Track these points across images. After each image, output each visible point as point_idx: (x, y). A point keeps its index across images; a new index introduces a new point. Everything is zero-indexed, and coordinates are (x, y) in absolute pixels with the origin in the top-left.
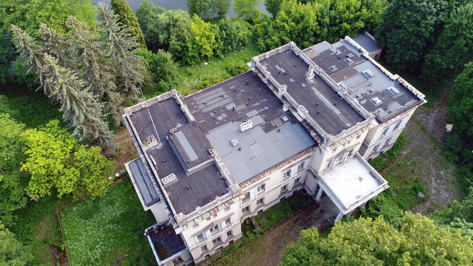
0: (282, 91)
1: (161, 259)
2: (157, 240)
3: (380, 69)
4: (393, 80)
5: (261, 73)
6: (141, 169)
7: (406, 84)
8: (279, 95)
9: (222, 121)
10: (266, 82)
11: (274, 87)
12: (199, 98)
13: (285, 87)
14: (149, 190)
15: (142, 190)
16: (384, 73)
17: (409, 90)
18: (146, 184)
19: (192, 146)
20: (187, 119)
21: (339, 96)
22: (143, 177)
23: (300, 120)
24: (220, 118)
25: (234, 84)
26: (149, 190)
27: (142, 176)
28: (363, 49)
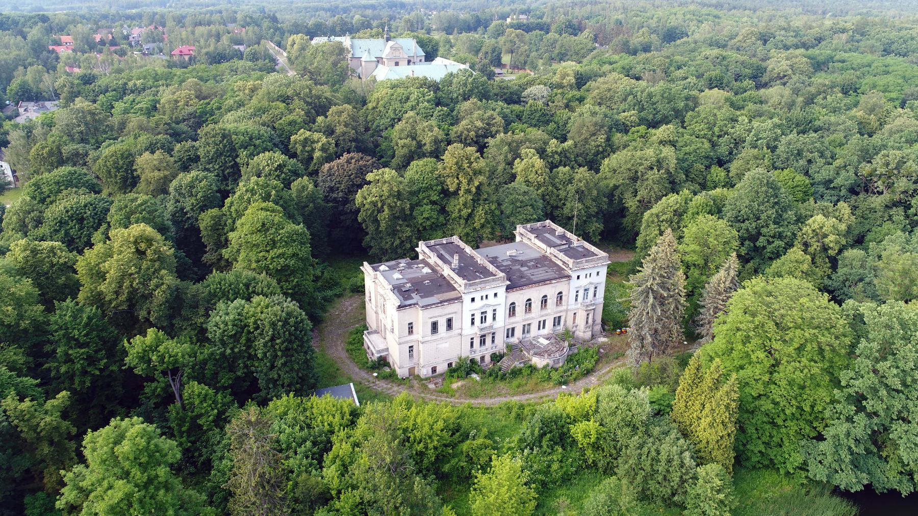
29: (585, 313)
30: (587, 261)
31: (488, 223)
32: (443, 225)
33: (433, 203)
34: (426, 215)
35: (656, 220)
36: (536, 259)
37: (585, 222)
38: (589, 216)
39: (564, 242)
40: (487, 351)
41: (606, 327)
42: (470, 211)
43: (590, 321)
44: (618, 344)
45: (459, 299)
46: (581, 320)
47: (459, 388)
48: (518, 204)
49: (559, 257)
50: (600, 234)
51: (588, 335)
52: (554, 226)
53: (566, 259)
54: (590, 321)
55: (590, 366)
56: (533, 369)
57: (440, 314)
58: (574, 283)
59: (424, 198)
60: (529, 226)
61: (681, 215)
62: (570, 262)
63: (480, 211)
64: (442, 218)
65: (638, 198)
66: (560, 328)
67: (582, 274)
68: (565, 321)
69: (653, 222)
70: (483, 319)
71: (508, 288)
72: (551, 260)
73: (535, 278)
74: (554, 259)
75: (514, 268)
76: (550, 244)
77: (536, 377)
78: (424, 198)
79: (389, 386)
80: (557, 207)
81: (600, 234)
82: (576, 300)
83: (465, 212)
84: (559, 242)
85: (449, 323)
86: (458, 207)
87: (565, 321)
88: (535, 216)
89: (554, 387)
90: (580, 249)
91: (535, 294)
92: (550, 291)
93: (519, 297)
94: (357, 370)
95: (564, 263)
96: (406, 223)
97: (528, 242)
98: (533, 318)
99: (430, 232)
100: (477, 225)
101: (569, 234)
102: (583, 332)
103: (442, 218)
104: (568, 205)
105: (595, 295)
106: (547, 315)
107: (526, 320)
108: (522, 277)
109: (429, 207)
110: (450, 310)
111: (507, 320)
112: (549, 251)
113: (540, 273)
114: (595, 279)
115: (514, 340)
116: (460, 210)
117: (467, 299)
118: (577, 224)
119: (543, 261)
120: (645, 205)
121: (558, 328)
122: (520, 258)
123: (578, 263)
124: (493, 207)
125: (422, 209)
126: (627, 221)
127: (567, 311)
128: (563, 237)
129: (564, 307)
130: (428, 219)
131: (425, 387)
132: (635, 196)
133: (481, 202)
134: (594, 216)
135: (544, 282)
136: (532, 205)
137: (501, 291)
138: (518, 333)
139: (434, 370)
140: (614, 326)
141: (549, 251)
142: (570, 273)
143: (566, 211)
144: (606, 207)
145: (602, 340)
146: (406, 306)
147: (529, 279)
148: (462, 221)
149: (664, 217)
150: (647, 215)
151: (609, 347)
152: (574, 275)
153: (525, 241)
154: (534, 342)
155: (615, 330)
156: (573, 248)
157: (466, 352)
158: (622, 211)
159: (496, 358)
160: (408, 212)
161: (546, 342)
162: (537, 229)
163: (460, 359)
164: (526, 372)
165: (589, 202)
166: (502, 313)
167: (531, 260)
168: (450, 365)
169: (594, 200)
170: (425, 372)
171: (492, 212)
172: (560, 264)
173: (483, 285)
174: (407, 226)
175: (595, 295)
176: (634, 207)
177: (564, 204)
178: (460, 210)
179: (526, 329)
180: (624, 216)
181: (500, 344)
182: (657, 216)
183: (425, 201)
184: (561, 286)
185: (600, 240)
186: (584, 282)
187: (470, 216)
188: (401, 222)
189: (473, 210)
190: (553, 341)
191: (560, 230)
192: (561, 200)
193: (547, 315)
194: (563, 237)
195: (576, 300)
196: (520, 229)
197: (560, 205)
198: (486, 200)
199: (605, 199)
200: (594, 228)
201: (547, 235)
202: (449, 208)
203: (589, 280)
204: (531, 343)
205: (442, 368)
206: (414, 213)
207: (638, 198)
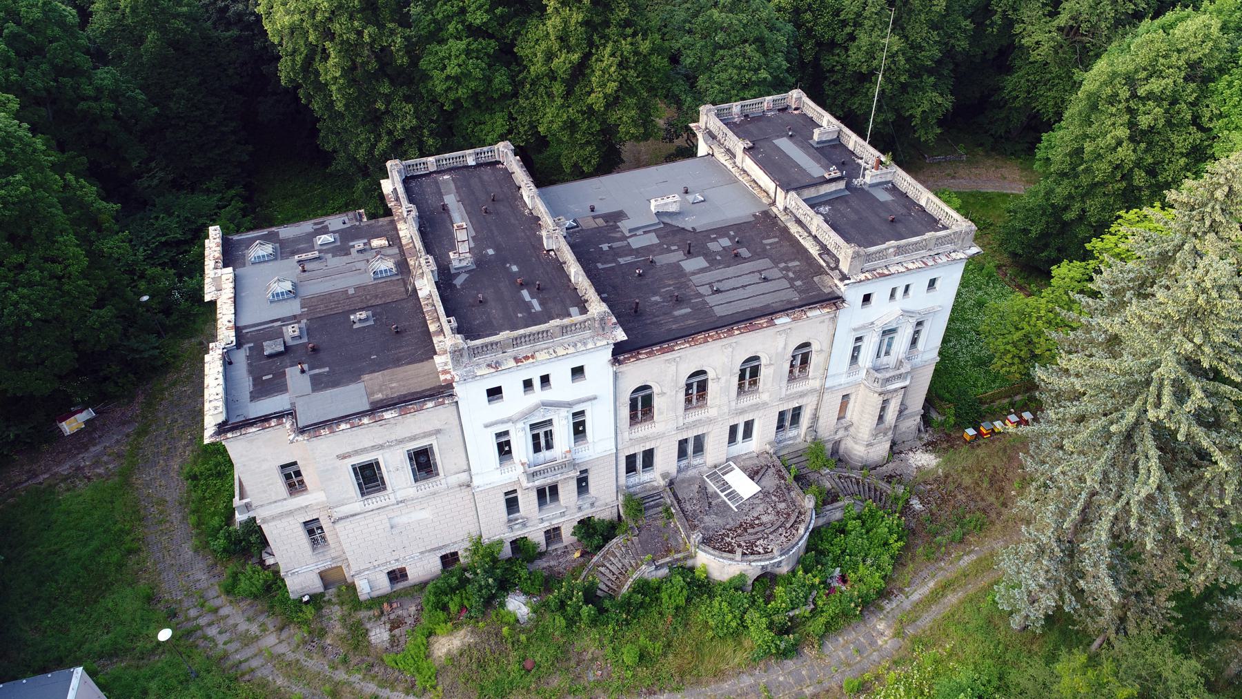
29: (877, 401)
30: (899, 251)
31: (632, 91)
32: (504, 96)
33: (474, 31)
34: (452, 70)
35: (1124, 93)
36: (739, 227)
37: (904, 87)
38: (917, 72)
39: (834, 172)
40: (567, 512)
41: (934, 415)
42: (575, 57)
43: (891, 415)
44: (967, 480)
45: (442, 392)
46: (863, 414)
47: (453, 659)
48: (719, 37)
49: (815, 231)
50: (940, 123)
51: (883, 448)
52: (811, 108)
53: (832, 239)
54: (891, 415)
55: (876, 580)
56: (701, 587)
57: (389, 441)
58: (852, 316)
59: (449, 18)
60: (736, 107)
61: (1207, 79)
62: (845, 252)
63: (606, 60)
64: (500, 79)
65: (1063, 19)
66: (799, 435)
67: (880, 290)
68: (815, 418)
69: (1113, 99)
70: (541, 439)
71: (620, 352)
72: (785, 230)
73: (721, 306)
74: (794, 229)
75: (663, 259)
76: (789, 179)
77: (711, 612)
78: (449, 18)
79: (254, 629)
80: (833, 44)
81: (940, 123)
82: (854, 358)
83: (564, 62)
84: (815, 169)
85: (423, 463)
86: (543, 46)
87: (815, 418)
88: (763, 74)
89: (753, 663)
90: (884, 196)
91: (718, 357)
92: (771, 344)
93: (664, 371)
94: (187, 551)
95: (824, 250)
96: (404, 90)
97: (725, 171)
98: (710, 421)
99: (476, 115)
100: (596, 99)
101: (853, 140)
102: (864, 445)
103: (500, 79)
104: (863, 39)
105: (914, 342)
106: (756, 407)
107: (687, 427)
108: (679, 301)
109: (462, 45)
110: (418, 426)
111: (626, 435)
112: (780, 203)
113: (742, 284)
114: (920, 300)
115: (653, 478)
116: (550, 56)
117: (470, 394)
118: (882, 92)
119: (760, 235)
120: (1081, 47)
121: (792, 433)
122: (688, 223)
123: (869, 258)
124: (645, 47)
125: (442, 51)
126: (1014, 84)
127: (821, 392)
128: (833, 151)
129: (813, 382)
130: (457, 79)
131: (357, 635)
132: (1054, 14)
133: (612, 31)
134: (930, 72)
135: (747, 319)
136: (760, 41)
137: (598, 360)
138: (666, 461)
139: (396, 576)
140: (957, 416)
141: (786, 202)
142: (842, 288)
143: (855, 56)
144: (964, 44)
145: (923, 460)
146: (249, 423)
147: (702, 309)
148: (558, 88)
149: (1155, 85)
150: (1094, 77)
151: (937, 489)
152: (853, 295)
153: (721, 157)
154: (712, 487)
155: (960, 426)
156: (861, 192)
157: (496, 528)
158: (1005, 54)
159: (594, 533)
160: (402, 60)
161: (744, 487)
162: (762, 117)
163: (478, 542)
164: (672, 598)
165: (919, 31)
166: (604, 423)
167: (721, 231)
168: (449, 560)
169: (934, 26)
170: (371, 583)
171: (643, 60)
172: (814, 251)
173: (524, 350)
174: (407, 99)
175: (914, 342)
176: (1045, 48)
177: (852, 38)
178: (550, 56)
179: (690, 448)
180: (1010, 70)
181: (605, 500)
182: (1130, 80)
183: (451, 28)
184: (811, 326)
185: (939, 138)
186: (884, 311)
187: (580, 71)
188: (385, 89)
189: (587, 56)
190: (771, 481)
191: (827, 124)
192: (844, 23)
193: (756, 407)
194: (833, 151)
195: (854, 358)
196: (707, 118)
197: (839, 39)
198: (627, 23)
199: (967, 24)
200: (926, 106)
201: (784, 144)
202: (522, 50)
203: (900, 303)
204: (703, 488)
205: (424, 567)
206: (423, 64)
207: (1063, 19)
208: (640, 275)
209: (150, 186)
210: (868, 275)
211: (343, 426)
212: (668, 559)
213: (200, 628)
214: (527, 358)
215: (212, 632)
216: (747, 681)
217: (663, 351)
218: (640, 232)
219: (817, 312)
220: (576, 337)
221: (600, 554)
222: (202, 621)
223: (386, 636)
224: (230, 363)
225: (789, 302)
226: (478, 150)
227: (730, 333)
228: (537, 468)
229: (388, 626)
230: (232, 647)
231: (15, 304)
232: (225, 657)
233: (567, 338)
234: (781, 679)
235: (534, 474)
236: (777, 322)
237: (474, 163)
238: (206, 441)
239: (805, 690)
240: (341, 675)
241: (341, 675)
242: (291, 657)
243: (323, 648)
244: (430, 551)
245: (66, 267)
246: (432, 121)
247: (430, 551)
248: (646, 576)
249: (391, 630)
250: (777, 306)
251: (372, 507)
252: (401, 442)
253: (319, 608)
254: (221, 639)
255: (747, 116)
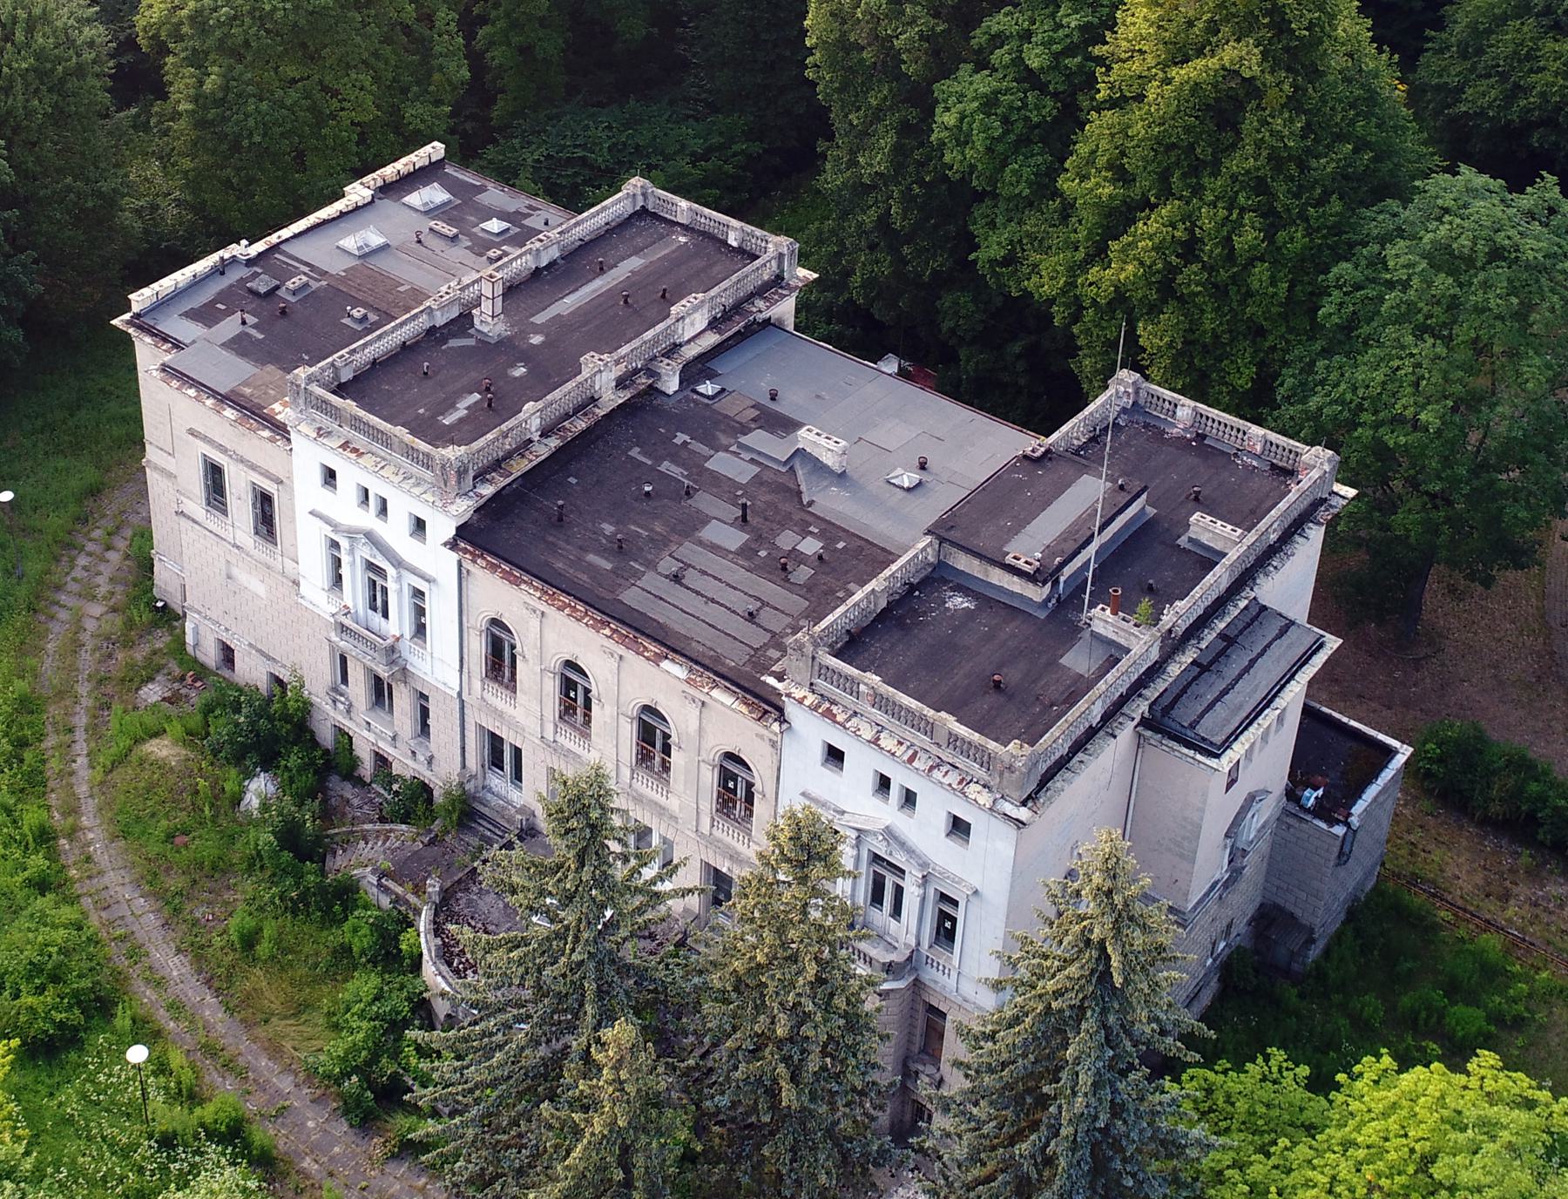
0: (601, 376)
1: (1390, 753)
2: (1339, 795)
3: (325, 222)
4: (372, 201)
5: (509, 456)
6: (1210, 697)
7: (389, 172)
8: (611, 399)
9: (820, 536)
10: (554, 442)
11: (576, 411)
12: (724, 647)
13: (590, 362)
14: (1268, 646)
15: (1284, 666)
16: (342, 214)
17: (410, 174)
18: (1252, 662)
19: (1048, 503)
20: (912, 588)
21: (552, 264)
22: (1237, 680)
23: (712, 339)
24: (810, 546)
25: (578, 563)
26: (1268, 646)
27: (1231, 686)
28: (226, 253)
30: (880, 702)
173: (360, 441)
203: (885, 813)
208: (648, 494)
209: (1294, 104)
210: (811, 699)
211: (192, 392)
212: (399, 890)
213: (82, 548)
214: (355, 450)
215: (82, 561)
216: (286, 1084)
217: (506, 576)
218: (747, 456)
219: (728, 699)
220: (416, 470)
221: (378, 826)
222: (90, 547)
223: (154, 698)
224: (222, 273)
225: (717, 659)
226: (749, 228)
227: (598, 626)
228: (354, 626)
229: (168, 694)
230: (74, 587)
231: (247, 116)
232: (58, 588)
233: (406, 463)
234: (310, 1124)
235: (343, 628)
236: (666, 664)
237: (735, 244)
238: (113, 322)
239: (308, 1159)
240: (83, 689)
241: (83, 689)
242: (85, 637)
243: (110, 656)
244: (259, 651)
245: (342, 109)
246: (921, 183)
247: (259, 651)
248: (363, 883)
249: (164, 699)
250: (695, 649)
251: (211, 526)
252: (253, 467)
253: (155, 625)
254: (78, 573)
255: (1201, 437)
